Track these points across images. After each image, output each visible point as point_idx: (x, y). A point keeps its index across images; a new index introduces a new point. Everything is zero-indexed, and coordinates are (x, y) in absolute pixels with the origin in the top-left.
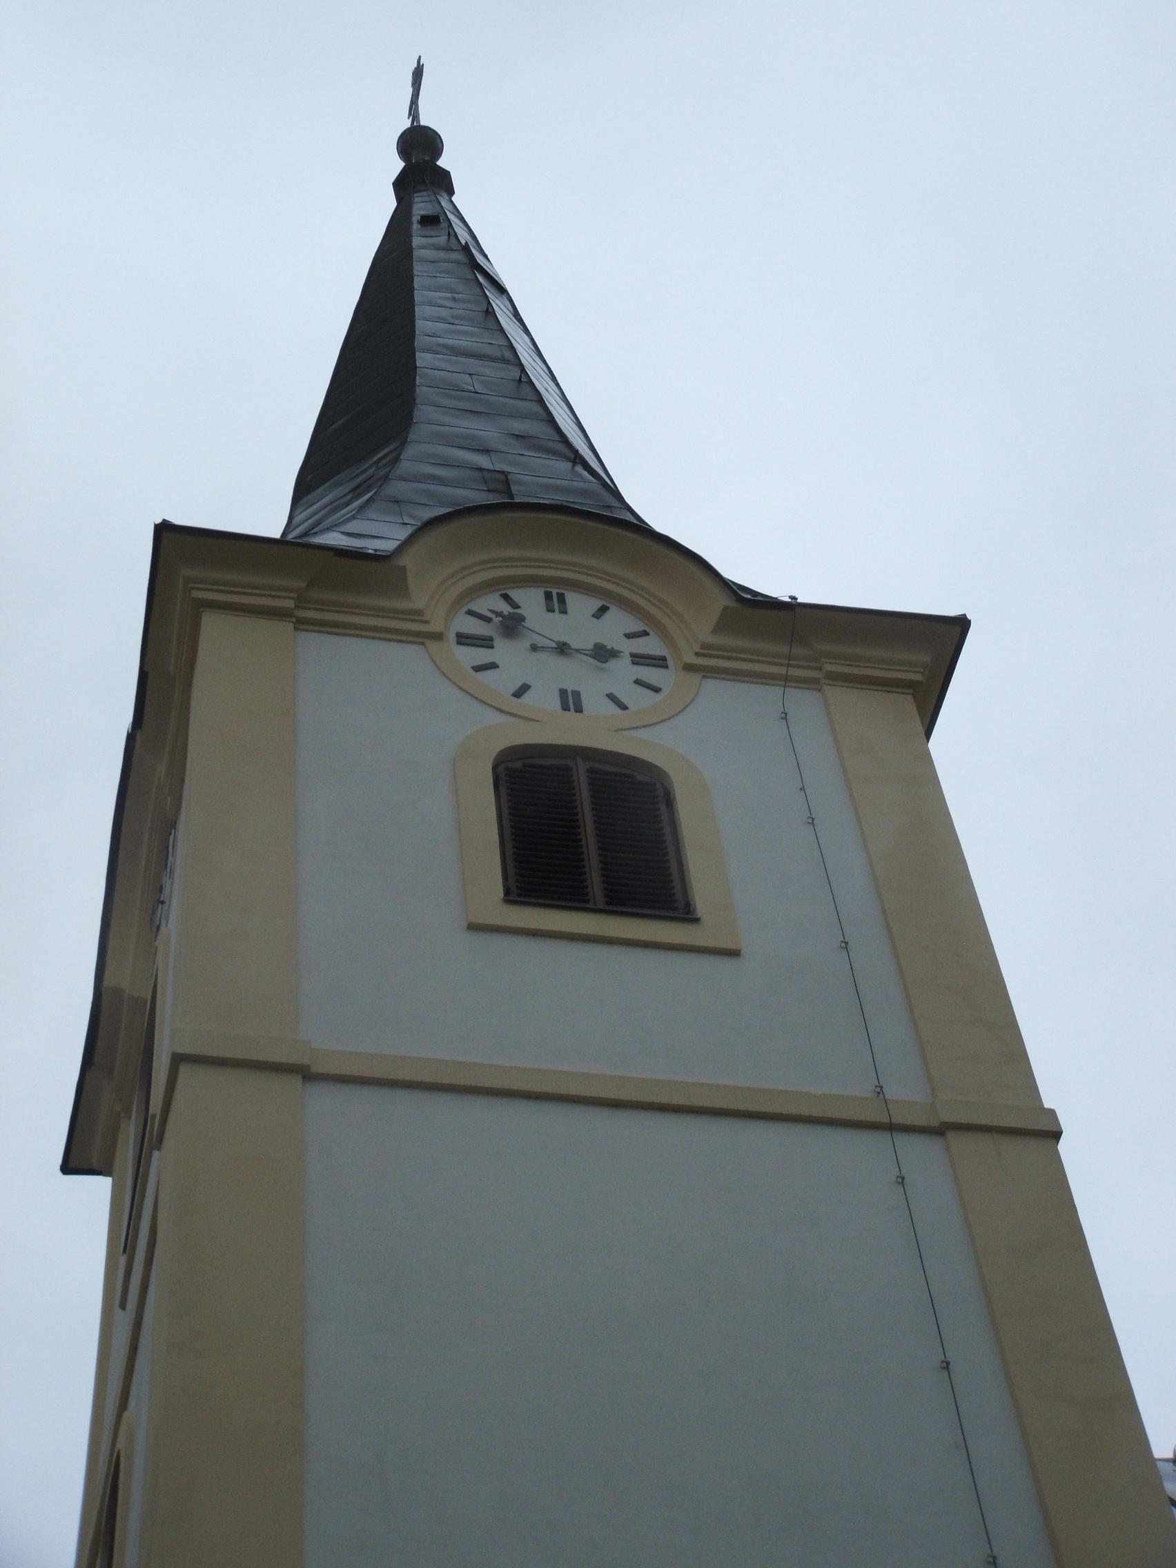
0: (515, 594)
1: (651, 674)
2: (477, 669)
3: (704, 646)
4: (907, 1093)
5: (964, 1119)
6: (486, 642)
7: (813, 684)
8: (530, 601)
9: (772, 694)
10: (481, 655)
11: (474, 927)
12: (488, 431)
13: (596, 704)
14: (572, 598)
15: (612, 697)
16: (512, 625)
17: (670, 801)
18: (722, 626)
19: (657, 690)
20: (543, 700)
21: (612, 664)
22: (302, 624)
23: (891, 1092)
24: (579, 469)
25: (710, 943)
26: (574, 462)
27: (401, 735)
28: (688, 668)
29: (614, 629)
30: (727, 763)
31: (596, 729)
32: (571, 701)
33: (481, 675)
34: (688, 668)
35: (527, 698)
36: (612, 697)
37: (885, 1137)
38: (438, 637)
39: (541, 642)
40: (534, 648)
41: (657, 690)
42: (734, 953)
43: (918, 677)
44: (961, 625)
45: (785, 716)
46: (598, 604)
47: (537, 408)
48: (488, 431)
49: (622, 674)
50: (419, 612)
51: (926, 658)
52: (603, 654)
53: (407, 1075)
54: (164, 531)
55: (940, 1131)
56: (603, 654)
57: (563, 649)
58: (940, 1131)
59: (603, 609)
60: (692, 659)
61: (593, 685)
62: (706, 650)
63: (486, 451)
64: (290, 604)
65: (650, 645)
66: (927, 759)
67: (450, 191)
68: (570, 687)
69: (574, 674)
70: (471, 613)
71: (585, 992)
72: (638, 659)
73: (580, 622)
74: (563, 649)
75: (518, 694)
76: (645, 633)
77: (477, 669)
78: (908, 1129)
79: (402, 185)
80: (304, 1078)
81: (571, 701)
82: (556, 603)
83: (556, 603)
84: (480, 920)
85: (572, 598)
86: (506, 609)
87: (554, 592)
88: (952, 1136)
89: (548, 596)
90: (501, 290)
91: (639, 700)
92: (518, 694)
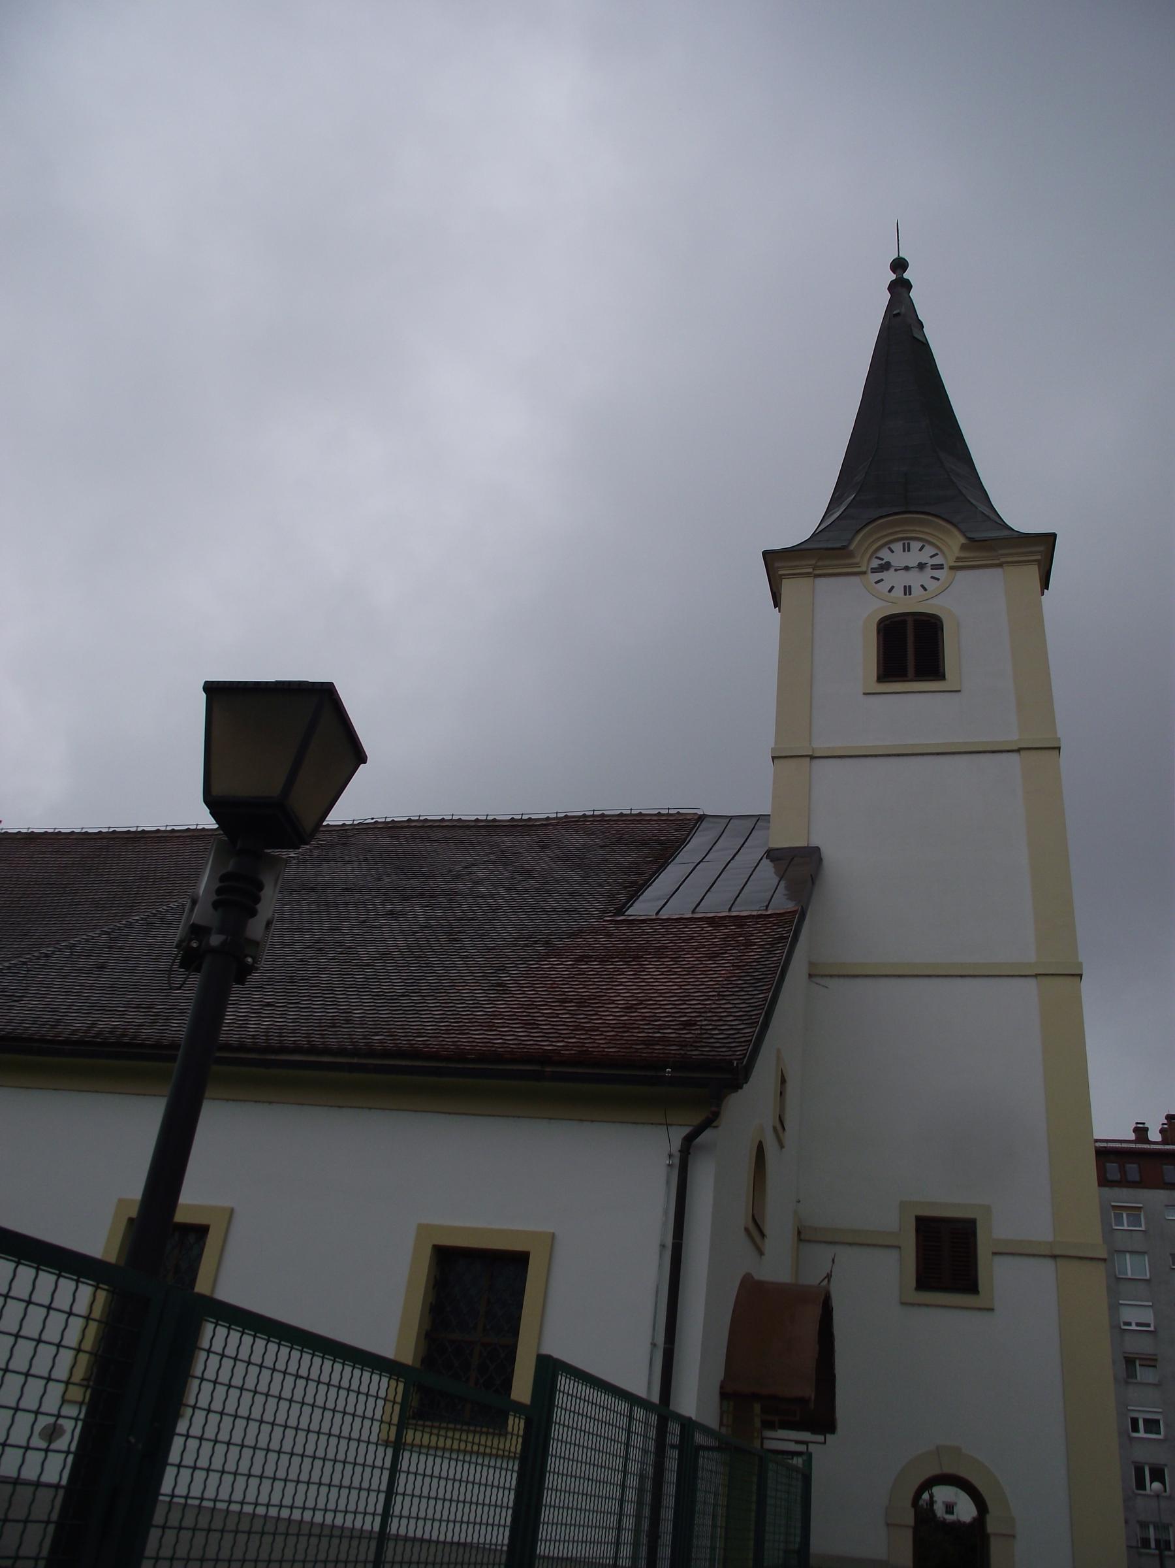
0: (880, 555)
1: (936, 573)
10: (878, 576)
13: (917, 591)
14: (893, 546)
16: (886, 567)
18: (963, 547)
20: (899, 592)
27: (850, 611)
28: (952, 568)
30: (971, 605)
32: (908, 590)
34: (952, 568)
38: (864, 573)
43: (1039, 557)
46: (920, 544)
49: (925, 577)
51: (1042, 548)
54: (766, 554)
55: (1018, 750)
56: (921, 566)
57: (907, 568)
58: (1018, 750)
61: (915, 579)
62: (958, 559)
65: (938, 560)
66: (1079, 990)
71: (914, 710)
73: (914, 557)
74: (907, 568)
75: (890, 591)
79: (892, 287)
80: (973, 544)
81: (908, 590)
82: (907, 548)
85: (893, 546)
91: (932, 586)
92: (890, 591)
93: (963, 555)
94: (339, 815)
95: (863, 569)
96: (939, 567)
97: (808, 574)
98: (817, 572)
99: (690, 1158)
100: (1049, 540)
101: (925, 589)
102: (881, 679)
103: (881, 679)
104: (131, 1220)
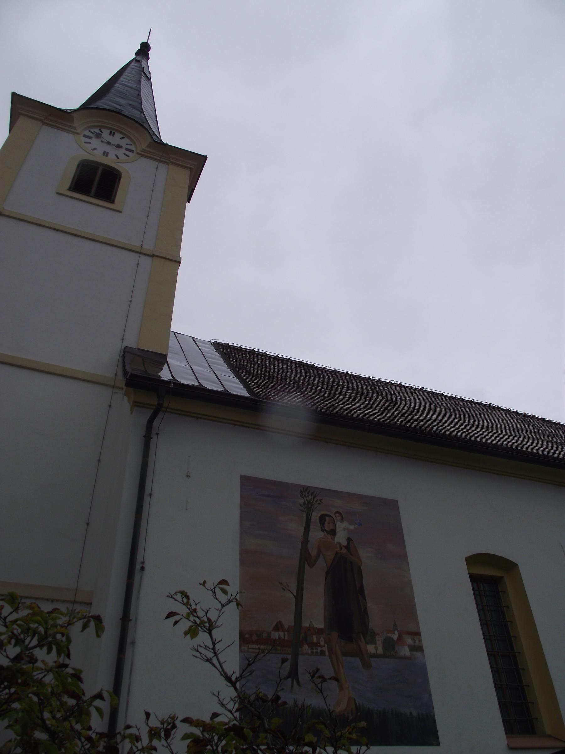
0: (102, 130)
1: (127, 153)
2: (85, 143)
3: (143, 149)
4: (148, 247)
5: (159, 255)
6: (90, 138)
7: (167, 163)
8: (106, 133)
9: (155, 164)
11: (58, 193)
12: (122, 101)
13: (112, 156)
15: (116, 156)
16: (98, 136)
17: (120, 180)
18: (149, 146)
19: (128, 156)
21: (120, 149)
22: (45, 124)
23: (144, 246)
24: (142, 115)
25: (116, 209)
26: (141, 112)
27: (68, 151)
28: (138, 154)
29: (124, 143)
30: (138, 175)
31: (110, 161)
32: (106, 154)
33: (86, 144)
35: (95, 151)
36: (116, 156)
37: (138, 255)
38: (78, 134)
39: (104, 140)
40: (102, 141)
41: (128, 156)
42: (120, 212)
44: (14, 95)
45: (157, 168)
47: (140, 101)
48: (122, 101)
50: (75, 127)
52: (118, 146)
53: (31, 220)
54: (205, 158)
55: (152, 256)
56: (118, 146)
57: (109, 143)
58: (152, 256)
59: (123, 138)
60: (139, 152)
62: (144, 151)
63: (120, 105)
64: (43, 118)
65: (132, 148)
67: (148, 58)
68: (107, 151)
69: (108, 148)
70: (90, 131)
71: (86, 213)
72: (127, 149)
73: (117, 139)
74: (109, 143)
76: (131, 145)
77: (85, 143)
78: (145, 254)
79: (138, 53)
81: (106, 154)
82: (112, 134)
83: (112, 134)
84: (60, 192)
86: (99, 132)
87: (113, 132)
88: (154, 258)
89: (111, 132)
90: (149, 79)
93: (147, 149)
94: (245, 393)
95: (79, 131)
96: (132, 151)
97: (40, 120)
98: (46, 122)
99: (153, 442)
100: (194, 164)
101: (118, 158)
102: (70, 189)
103: (70, 189)
104: (144, 436)
